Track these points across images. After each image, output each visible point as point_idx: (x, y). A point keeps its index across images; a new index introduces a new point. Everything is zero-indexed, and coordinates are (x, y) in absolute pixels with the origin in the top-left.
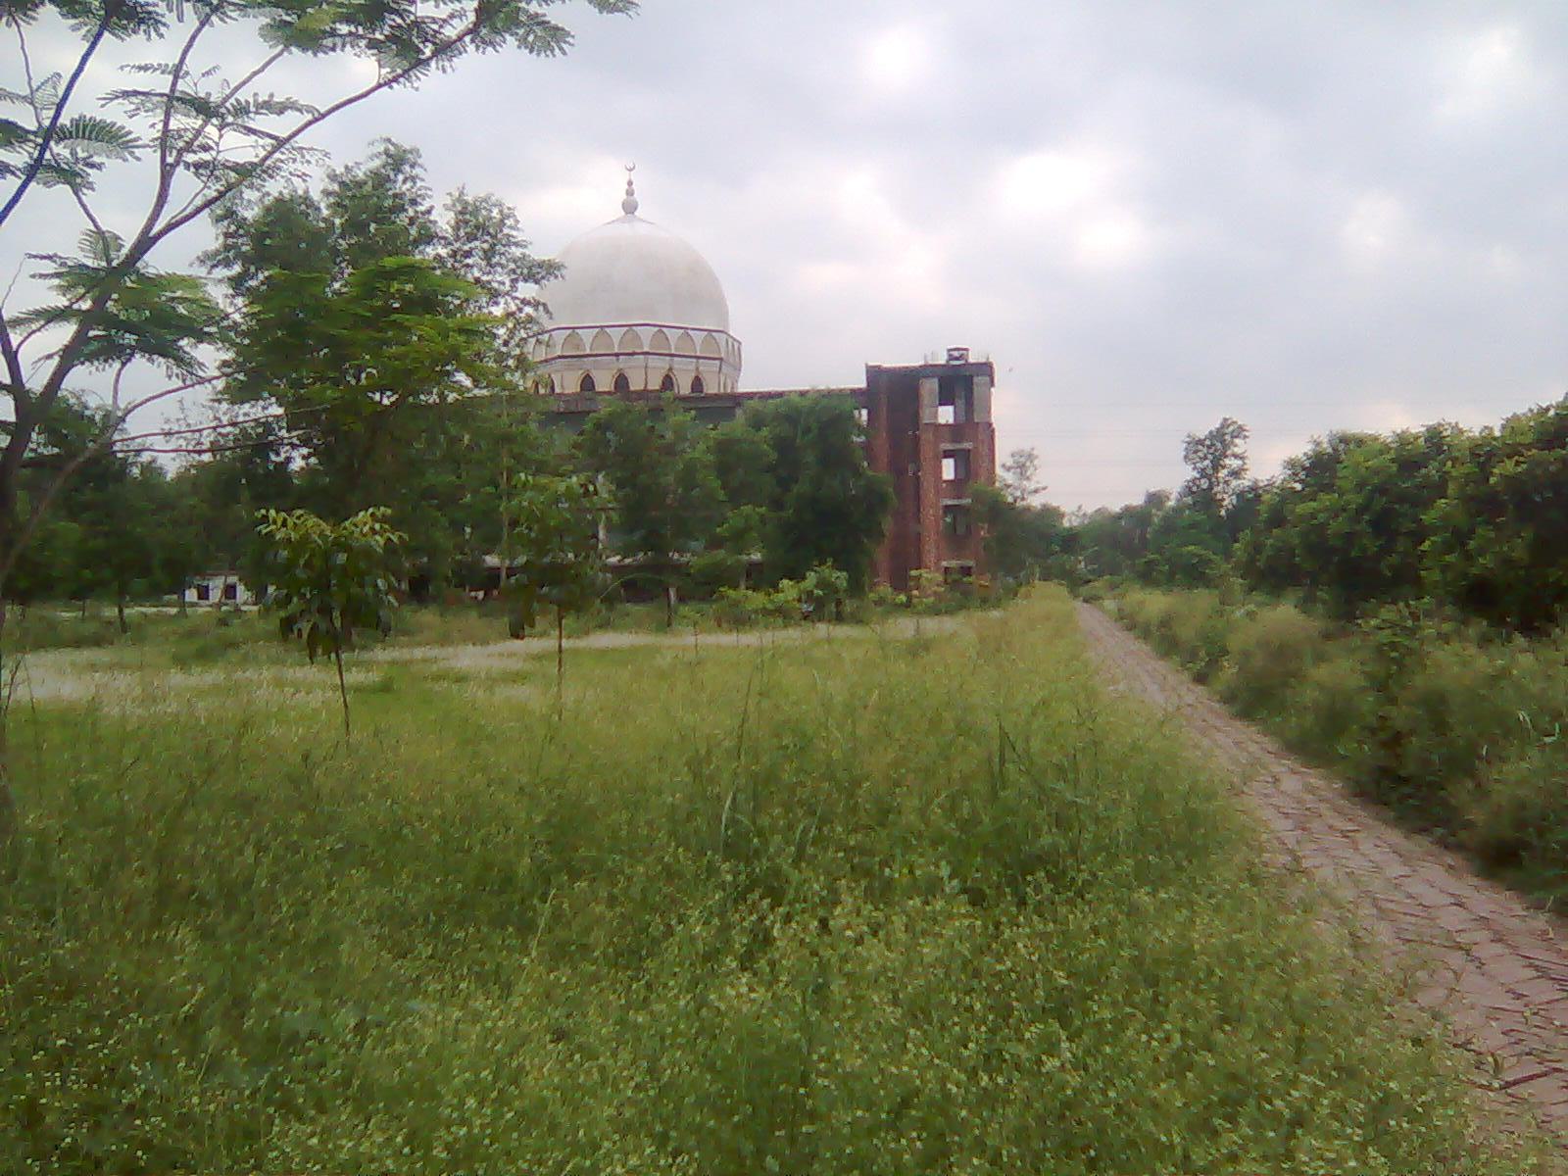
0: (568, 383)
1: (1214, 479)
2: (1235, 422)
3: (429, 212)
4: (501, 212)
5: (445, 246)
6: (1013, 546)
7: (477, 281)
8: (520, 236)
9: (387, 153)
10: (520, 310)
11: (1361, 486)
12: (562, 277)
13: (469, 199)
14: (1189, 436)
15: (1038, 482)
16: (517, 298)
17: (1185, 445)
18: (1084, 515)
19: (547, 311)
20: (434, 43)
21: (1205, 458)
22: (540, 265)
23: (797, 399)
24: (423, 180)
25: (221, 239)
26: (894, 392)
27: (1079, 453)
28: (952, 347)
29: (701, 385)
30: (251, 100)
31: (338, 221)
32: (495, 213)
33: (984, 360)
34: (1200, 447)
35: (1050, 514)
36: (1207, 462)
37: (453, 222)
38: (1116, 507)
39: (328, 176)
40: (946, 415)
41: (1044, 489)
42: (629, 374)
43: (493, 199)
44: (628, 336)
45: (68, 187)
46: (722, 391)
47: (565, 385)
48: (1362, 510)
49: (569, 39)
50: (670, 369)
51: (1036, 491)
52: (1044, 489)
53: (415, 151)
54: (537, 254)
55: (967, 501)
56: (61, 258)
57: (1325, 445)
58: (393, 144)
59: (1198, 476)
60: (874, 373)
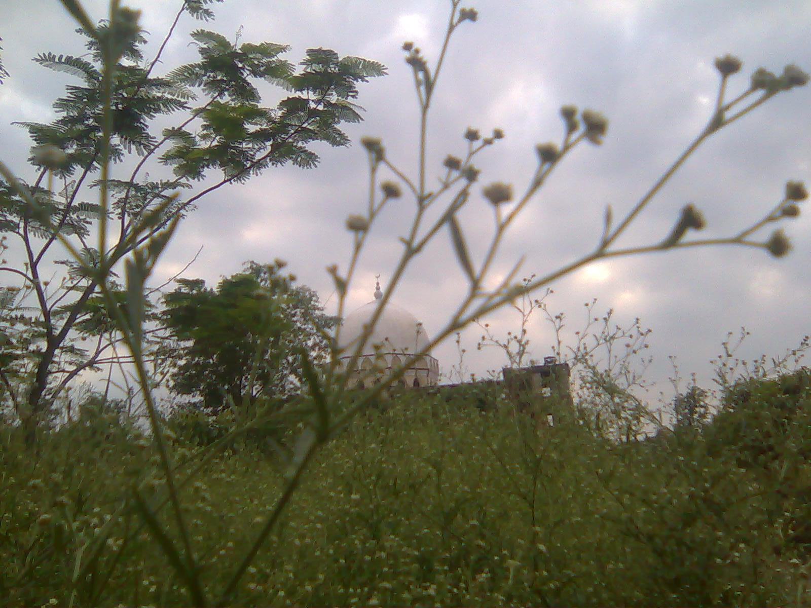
4: (310, 294)
8: (320, 306)
9: (251, 267)
20: (252, 161)
28: (547, 356)
30: (159, 182)
32: (307, 294)
45: (76, 235)
49: (318, 159)
56: (70, 263)
58: (255, 264)
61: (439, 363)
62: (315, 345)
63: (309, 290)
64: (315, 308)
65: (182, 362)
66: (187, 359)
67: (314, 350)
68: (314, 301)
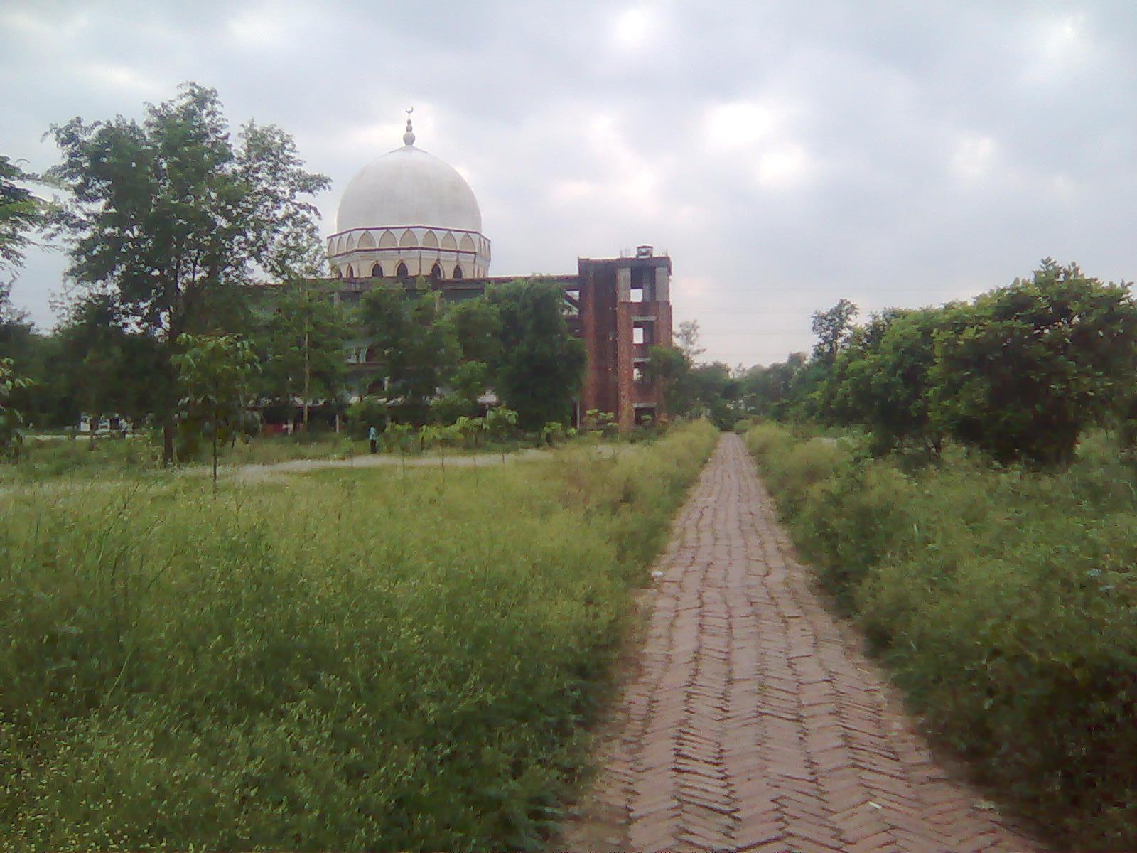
0: (363, 270)
1: (834, 345)
2: (849, 302)
3: (226, 137)
4: (281, 139)
5: (240, 164)
6: (683, 390)
7: (266, 190)
8: (296, 157)
9: (192, 93)
10: (297, 212)
11: (896, 348)
12: (330, 188)
13: (257, 128)
14: (816, 313)
15: (699, 346)
16: (295, 204)
17: (813, 319)
18: (744, 370)
19: (317, 214)
21: (828, 329)
22: (312, 179)
23: (522, 283)
24: (221, 113)
25: (67, 157)
26: (598, 279)
27: (737, 324)
29: (460, 271)
31: (159, 145)
32: (277, 139)
33: (664, 256)
34: (824, 321)
35: (719, 369)
36: (829, 332)
37: (246, 147)
38: (766, 365)
39: (150, 111)
40: (636, 296)
41: (704, 350)
42: (407, 263)
43: (276, 129)
44: (407, 235)
46: (476, 276)
47: (361, 271)
48: (897, 366)
50: (438, 260)
51: (698, 352)
52: (704, 350)
53: (213, 92)
54: (309, 170)
55: (648, 360)
57: (881, 318)
58: (197, 87)
59: (823, 342)
60: (584, 265)
61: (492, 245)
62: (288, 217)
63: (280, 132)
64: (288, 160)
65: (86, 235)
66: (93, 230)
67: (284, 224)
68: (289, 150)
